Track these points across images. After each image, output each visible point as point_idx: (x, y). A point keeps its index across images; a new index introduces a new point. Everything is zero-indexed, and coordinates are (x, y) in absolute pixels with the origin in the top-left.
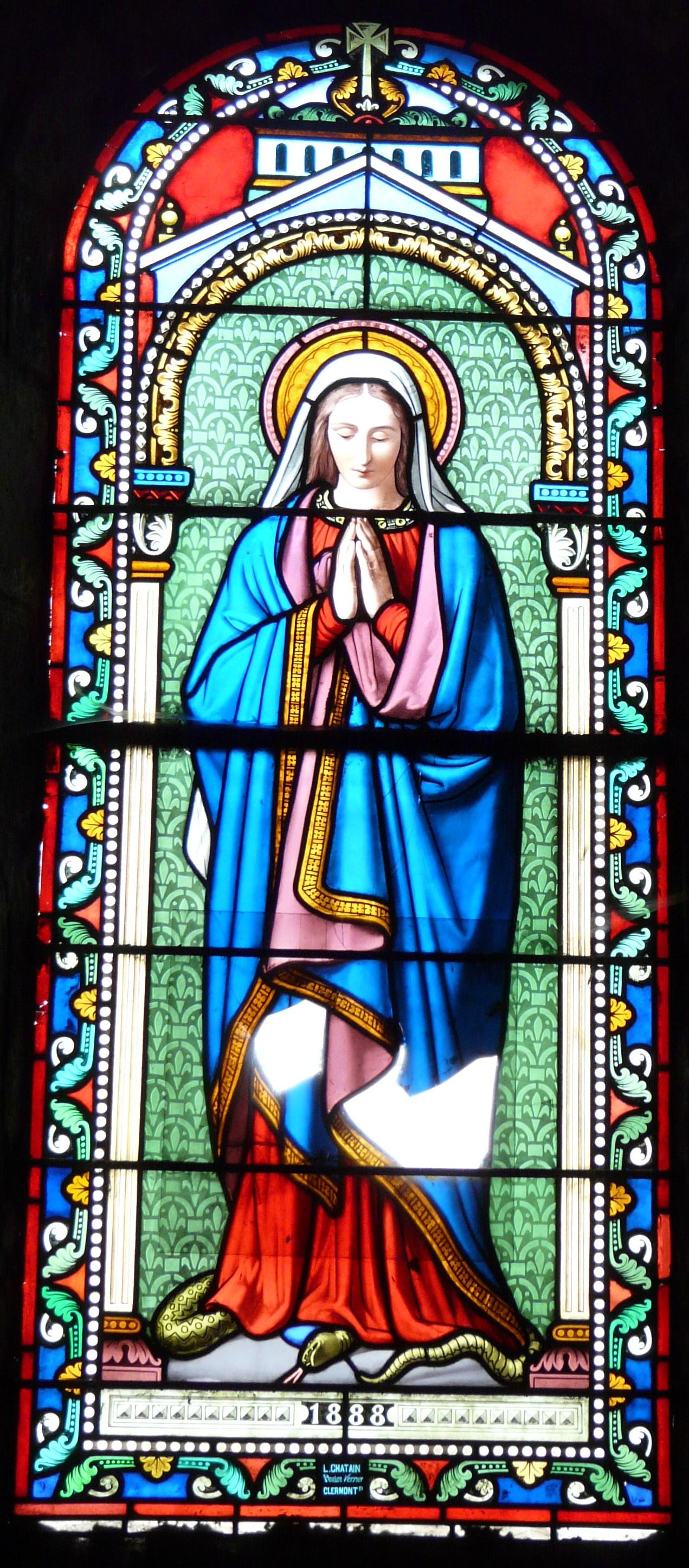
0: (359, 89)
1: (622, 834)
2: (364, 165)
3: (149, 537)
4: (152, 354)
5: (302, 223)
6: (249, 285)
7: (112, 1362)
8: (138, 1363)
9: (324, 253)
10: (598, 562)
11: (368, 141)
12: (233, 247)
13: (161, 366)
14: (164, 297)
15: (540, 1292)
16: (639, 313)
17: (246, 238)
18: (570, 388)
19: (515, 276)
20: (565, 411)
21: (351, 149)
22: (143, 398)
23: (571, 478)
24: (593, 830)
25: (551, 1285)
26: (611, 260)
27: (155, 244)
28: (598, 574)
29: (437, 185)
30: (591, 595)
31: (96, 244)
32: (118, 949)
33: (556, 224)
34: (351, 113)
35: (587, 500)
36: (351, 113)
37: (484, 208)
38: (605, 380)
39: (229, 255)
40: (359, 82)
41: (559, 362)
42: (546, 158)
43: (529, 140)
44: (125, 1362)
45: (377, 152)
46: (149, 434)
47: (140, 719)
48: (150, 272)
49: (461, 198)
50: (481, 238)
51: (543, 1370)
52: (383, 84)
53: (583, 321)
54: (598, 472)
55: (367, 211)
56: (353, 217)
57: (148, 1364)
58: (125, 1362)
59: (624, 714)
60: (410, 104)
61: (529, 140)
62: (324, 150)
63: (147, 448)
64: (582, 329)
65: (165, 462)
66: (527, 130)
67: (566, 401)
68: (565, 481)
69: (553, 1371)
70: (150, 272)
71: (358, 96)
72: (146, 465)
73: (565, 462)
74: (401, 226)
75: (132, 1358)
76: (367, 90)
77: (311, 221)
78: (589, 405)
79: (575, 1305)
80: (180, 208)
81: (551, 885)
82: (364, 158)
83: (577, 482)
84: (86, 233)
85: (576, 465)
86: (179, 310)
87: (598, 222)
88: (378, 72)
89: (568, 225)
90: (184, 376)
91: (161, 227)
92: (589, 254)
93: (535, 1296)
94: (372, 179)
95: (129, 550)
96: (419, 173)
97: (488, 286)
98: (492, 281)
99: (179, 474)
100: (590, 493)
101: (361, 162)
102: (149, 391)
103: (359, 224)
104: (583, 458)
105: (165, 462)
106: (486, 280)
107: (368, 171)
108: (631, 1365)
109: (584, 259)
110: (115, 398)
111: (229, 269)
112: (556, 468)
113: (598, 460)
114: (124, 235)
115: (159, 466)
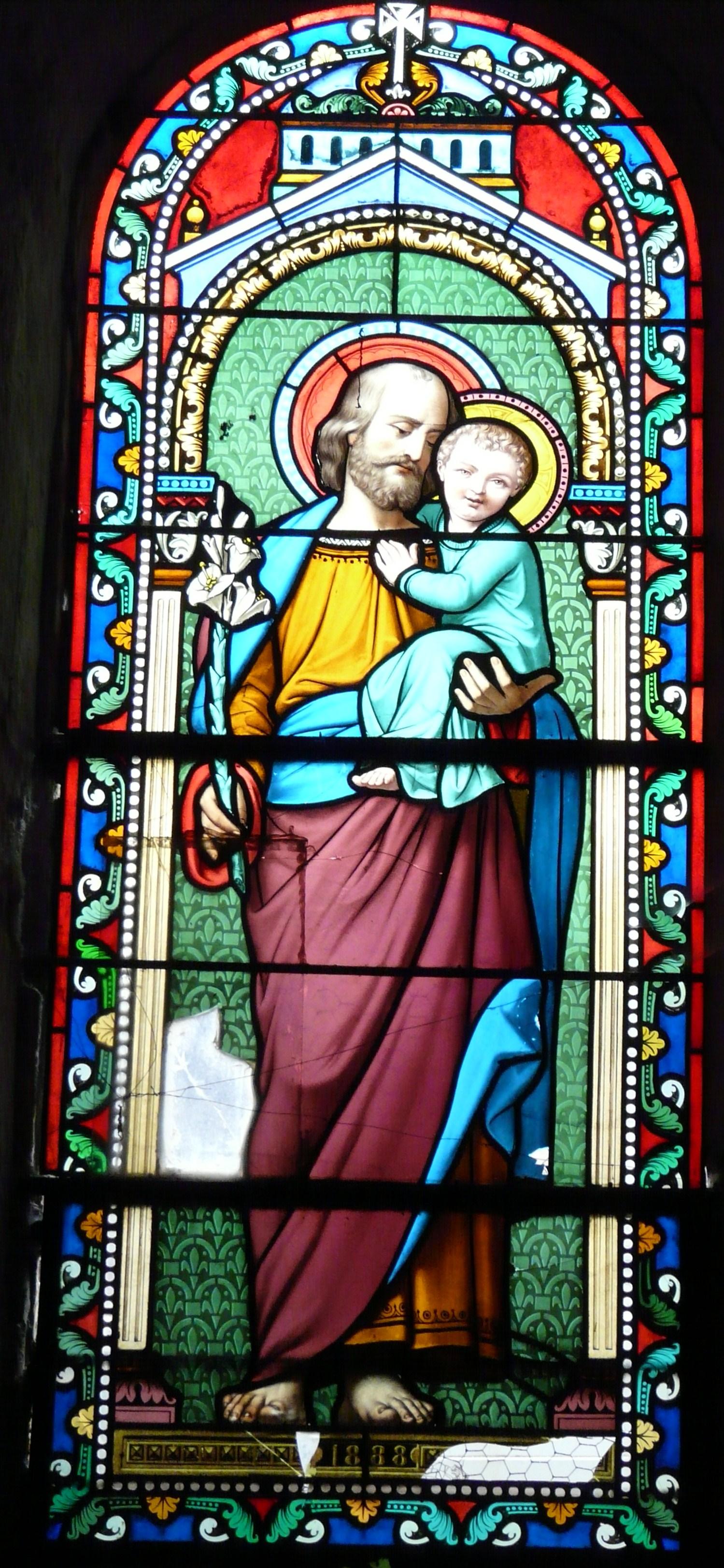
0: (390, 75)
1: (656, 653)
2: (393, 156)
3: (171, 545)
4: (177, 357)
5: (330, 221)
6: (275, 284)
7: (124, 1402)
8: (151, 1403)
9: (351, 251)
10: (636, 563)
11: (397, 131)
12: (258, 246)
13: (186, 372)
14: (188, 302)
15: (567, 1248)
16: (679, 312)
17: (272, 238)
18: (606, 384)
19: (548, 270)
20: (601, 409)
21: (379, 138)
22: (167, 403)
23: (607, 478)
24: (629, 634)
25: (579, 1240)
26: (649, 253)
27: (182, 244)
28: (636, 576)
29: (466, 177)
30: (627, 597)
31: (123, 236)
32: (135, 964)
33: (590, 213)
34: (381, 101)
35: (623, 500)
36: (381, 101)
37: (517, 200)
38: (642, 375)
39: (255, 255)
40: (391, 67)
41: (594, 359)
42: (583, 147)
43: (565, 128)
44: (138, 1402)
45: (405, 141)
46: (173, 439)
47: (159, 729)
48: (174, 273)
49: (492, 190)
50: (513, 232)
51: (567, 1411)
52: (416, 66)
53: (619, 322)
54: (635, 470)
55: (395, 205)
56: (383, 213)
57: (162, 1403)
58: (138, 1402)
59: (663, 719)
60: (444, 91)
61: (565, 128)
62: (351, 140)
63: (171, 454)
64: (618, 330)
65: (188, 468)
66: (564, 119)
67: (602, 399)
68: (601, 481)
69: (579, 1410)
70: (174, 273)
71: (388, 82)
72: (170, 471)
73: (602, 461)
74: (431, 220)
75: (145, 1397)
76: (399, 75)
77: (339, 219)
78: (627, 400)
79: (602, 1345)
80: (206, 203)
81: (575, 1301)
82: (393, 148)
83: (613, 482)
84: (113, 224)
85: (614, 464)
86: (204, 313)
87: (635, 214)
88: (410, 57)
89: (603, 213)
90: (210, 379)
91: (188, 226)
92: (625, 246)
93: (562, 1251)
94: (402, 172)
95: (152, 558)
96: (448, 165)
97: (521, 281)
98: (526, 276)
99: (204, 480)
100: (629, 490)
101: (390, 153)
102: (174, 396)
103: (388, 220)
104: (620, 456)
105: (188, 468)
106: (519, 275)
107: (398, 163)
108: (666, 830)
109: (618, 249)
110: (140, 393)
111: (255, 270)
112: (593, 468)
113: (635, 457)
114: (151, 225)
115: (182, 472)
